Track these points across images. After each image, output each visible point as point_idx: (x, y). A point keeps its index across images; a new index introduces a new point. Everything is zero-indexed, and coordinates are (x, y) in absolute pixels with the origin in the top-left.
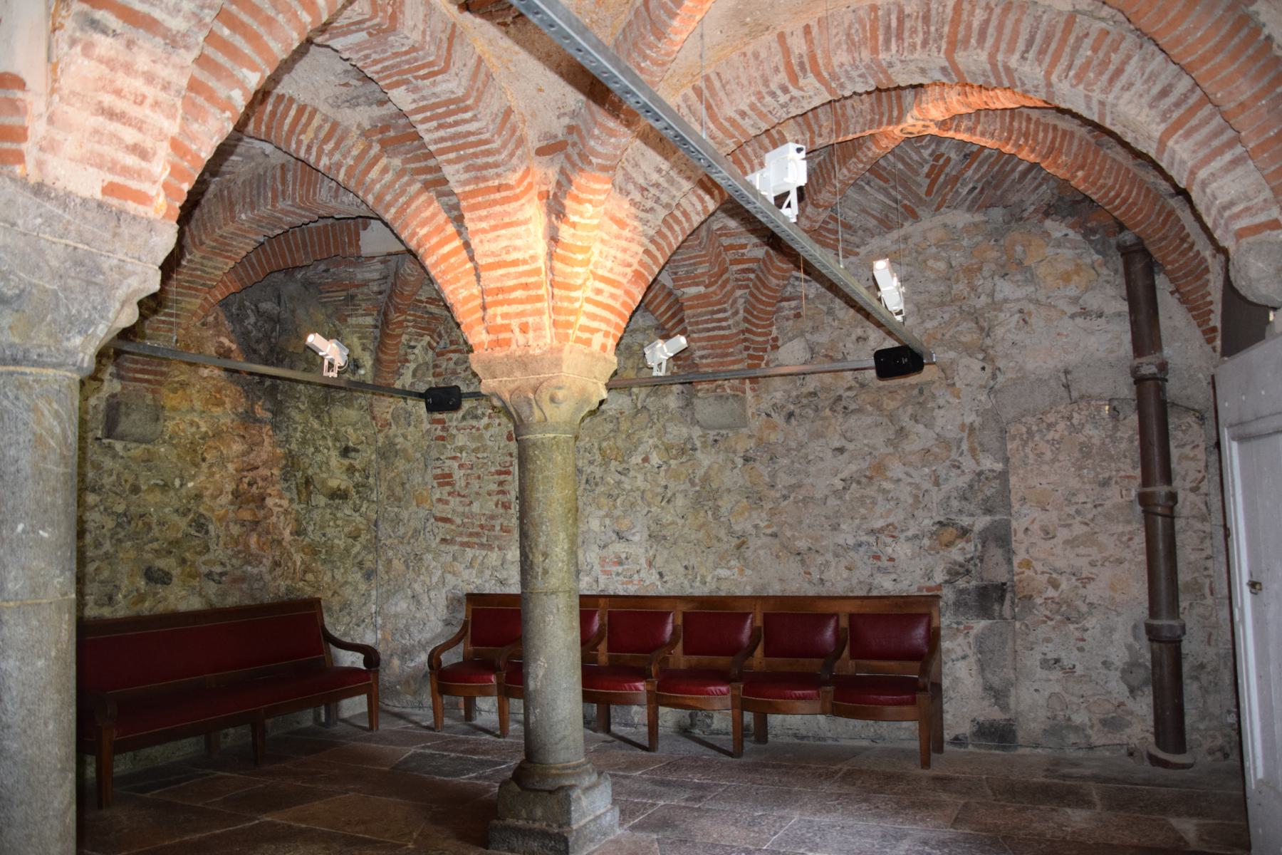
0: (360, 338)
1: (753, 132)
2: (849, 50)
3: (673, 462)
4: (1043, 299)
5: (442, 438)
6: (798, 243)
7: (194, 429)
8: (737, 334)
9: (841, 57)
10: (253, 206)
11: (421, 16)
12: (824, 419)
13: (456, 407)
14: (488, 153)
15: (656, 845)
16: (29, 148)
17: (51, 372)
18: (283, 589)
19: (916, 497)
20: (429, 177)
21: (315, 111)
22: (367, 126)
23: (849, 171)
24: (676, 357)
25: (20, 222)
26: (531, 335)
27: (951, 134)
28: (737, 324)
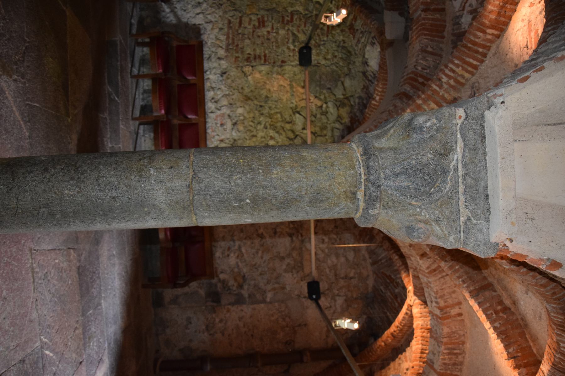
5: (283, 21)
19: (255, 265)
21: (473, 74)
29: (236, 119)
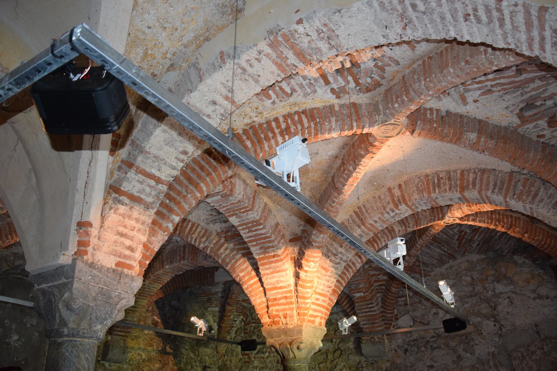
0: (213, 317)
1: (380, 229)
2: (418, 193)
4: (519, 292)
5: (248, 362)
7: (139, 357)
8: (379, 313)
9: (416, 196)
11: (242, 188)
12: (423, 351)
13: (254, 349)
14: (270, 242)
16: (90, 249)
17: (87, 340)
20: (244, 251)
21: (199, 225)
22: (219, 230)
23: (423, 240)
24: (352, 325)
25: (83, 278)
26: (288, 319)
27: (465, 222)
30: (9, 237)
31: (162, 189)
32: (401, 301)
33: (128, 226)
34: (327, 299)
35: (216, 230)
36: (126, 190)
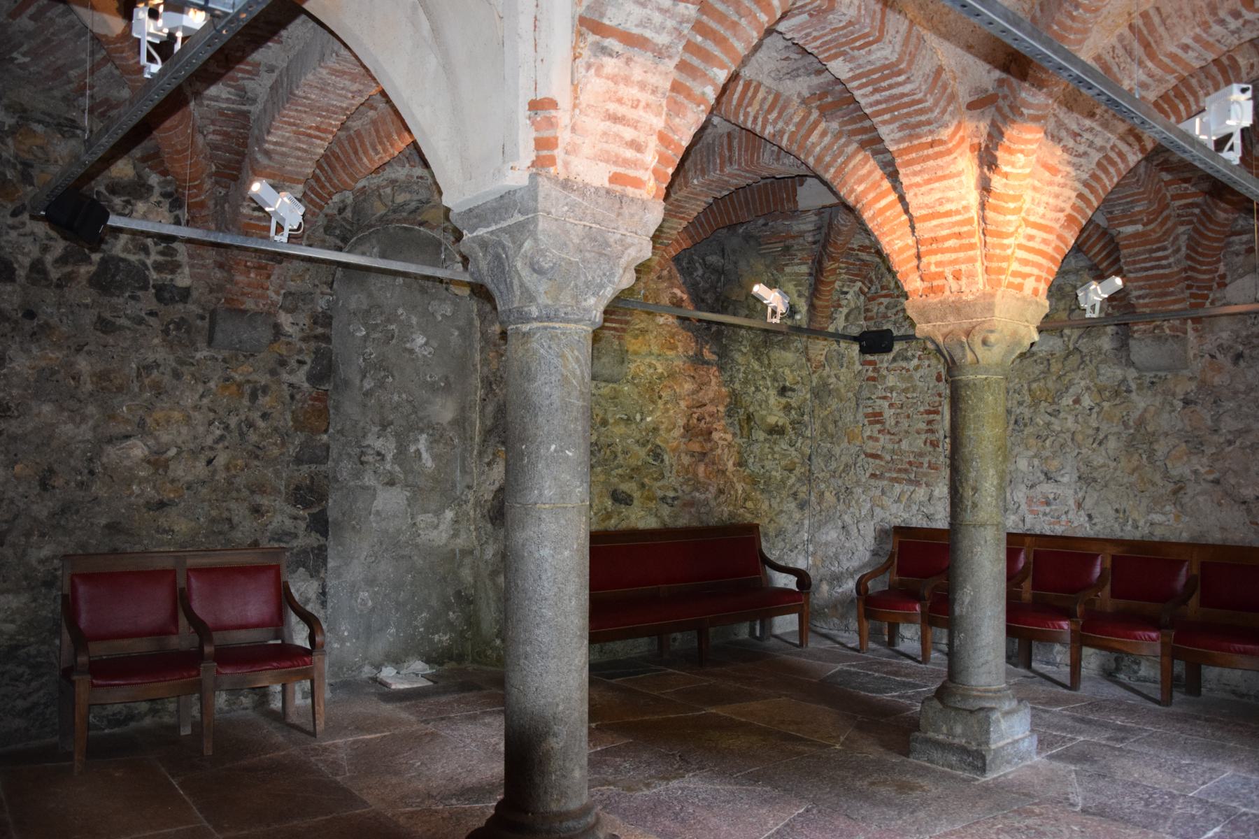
0: (796, 286)
1: (1197, 64)
3: (1106, 405)
5: (874, 379)
6: (1241, 185)
7: (652, 371)
8: (1179, 272)
10: (703, 172)
13: (888, 349)
15: (1073, 775)
16: (559, 153)
17: (572, 326)
18: (726, 515)
20: (864, 137)
21: (759, 84)
22: (806, 94)
24: (1111, 298)
25: (553, 211)
26: (964, 281)
28: (1178, 262)
29: (1039, 474)
30: (379, 148)
31: (686, 12)
32: (1238, 242)
33: (625, 100)
34: (1052, 237)
35: (799, 94)
36: (613, 23)
